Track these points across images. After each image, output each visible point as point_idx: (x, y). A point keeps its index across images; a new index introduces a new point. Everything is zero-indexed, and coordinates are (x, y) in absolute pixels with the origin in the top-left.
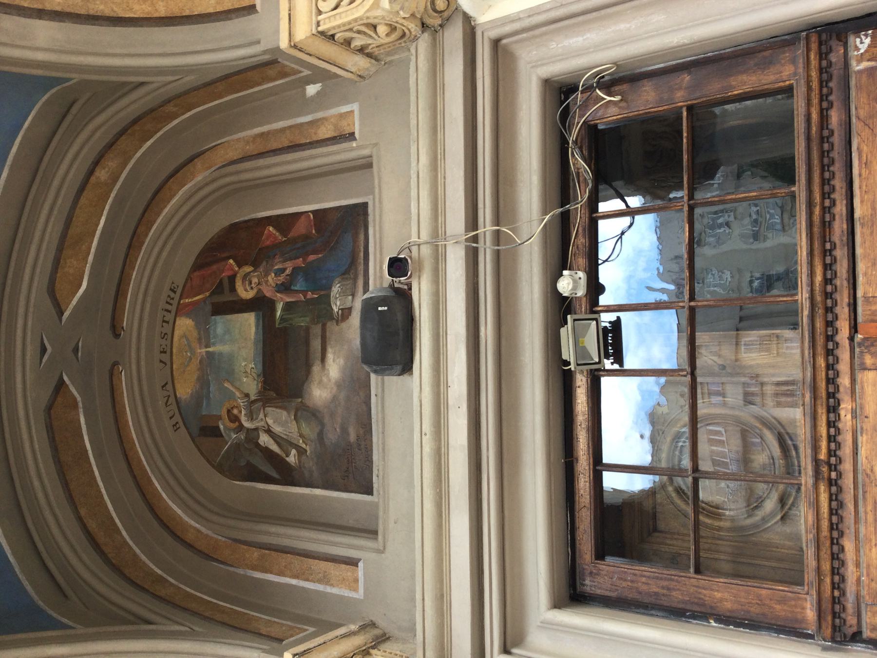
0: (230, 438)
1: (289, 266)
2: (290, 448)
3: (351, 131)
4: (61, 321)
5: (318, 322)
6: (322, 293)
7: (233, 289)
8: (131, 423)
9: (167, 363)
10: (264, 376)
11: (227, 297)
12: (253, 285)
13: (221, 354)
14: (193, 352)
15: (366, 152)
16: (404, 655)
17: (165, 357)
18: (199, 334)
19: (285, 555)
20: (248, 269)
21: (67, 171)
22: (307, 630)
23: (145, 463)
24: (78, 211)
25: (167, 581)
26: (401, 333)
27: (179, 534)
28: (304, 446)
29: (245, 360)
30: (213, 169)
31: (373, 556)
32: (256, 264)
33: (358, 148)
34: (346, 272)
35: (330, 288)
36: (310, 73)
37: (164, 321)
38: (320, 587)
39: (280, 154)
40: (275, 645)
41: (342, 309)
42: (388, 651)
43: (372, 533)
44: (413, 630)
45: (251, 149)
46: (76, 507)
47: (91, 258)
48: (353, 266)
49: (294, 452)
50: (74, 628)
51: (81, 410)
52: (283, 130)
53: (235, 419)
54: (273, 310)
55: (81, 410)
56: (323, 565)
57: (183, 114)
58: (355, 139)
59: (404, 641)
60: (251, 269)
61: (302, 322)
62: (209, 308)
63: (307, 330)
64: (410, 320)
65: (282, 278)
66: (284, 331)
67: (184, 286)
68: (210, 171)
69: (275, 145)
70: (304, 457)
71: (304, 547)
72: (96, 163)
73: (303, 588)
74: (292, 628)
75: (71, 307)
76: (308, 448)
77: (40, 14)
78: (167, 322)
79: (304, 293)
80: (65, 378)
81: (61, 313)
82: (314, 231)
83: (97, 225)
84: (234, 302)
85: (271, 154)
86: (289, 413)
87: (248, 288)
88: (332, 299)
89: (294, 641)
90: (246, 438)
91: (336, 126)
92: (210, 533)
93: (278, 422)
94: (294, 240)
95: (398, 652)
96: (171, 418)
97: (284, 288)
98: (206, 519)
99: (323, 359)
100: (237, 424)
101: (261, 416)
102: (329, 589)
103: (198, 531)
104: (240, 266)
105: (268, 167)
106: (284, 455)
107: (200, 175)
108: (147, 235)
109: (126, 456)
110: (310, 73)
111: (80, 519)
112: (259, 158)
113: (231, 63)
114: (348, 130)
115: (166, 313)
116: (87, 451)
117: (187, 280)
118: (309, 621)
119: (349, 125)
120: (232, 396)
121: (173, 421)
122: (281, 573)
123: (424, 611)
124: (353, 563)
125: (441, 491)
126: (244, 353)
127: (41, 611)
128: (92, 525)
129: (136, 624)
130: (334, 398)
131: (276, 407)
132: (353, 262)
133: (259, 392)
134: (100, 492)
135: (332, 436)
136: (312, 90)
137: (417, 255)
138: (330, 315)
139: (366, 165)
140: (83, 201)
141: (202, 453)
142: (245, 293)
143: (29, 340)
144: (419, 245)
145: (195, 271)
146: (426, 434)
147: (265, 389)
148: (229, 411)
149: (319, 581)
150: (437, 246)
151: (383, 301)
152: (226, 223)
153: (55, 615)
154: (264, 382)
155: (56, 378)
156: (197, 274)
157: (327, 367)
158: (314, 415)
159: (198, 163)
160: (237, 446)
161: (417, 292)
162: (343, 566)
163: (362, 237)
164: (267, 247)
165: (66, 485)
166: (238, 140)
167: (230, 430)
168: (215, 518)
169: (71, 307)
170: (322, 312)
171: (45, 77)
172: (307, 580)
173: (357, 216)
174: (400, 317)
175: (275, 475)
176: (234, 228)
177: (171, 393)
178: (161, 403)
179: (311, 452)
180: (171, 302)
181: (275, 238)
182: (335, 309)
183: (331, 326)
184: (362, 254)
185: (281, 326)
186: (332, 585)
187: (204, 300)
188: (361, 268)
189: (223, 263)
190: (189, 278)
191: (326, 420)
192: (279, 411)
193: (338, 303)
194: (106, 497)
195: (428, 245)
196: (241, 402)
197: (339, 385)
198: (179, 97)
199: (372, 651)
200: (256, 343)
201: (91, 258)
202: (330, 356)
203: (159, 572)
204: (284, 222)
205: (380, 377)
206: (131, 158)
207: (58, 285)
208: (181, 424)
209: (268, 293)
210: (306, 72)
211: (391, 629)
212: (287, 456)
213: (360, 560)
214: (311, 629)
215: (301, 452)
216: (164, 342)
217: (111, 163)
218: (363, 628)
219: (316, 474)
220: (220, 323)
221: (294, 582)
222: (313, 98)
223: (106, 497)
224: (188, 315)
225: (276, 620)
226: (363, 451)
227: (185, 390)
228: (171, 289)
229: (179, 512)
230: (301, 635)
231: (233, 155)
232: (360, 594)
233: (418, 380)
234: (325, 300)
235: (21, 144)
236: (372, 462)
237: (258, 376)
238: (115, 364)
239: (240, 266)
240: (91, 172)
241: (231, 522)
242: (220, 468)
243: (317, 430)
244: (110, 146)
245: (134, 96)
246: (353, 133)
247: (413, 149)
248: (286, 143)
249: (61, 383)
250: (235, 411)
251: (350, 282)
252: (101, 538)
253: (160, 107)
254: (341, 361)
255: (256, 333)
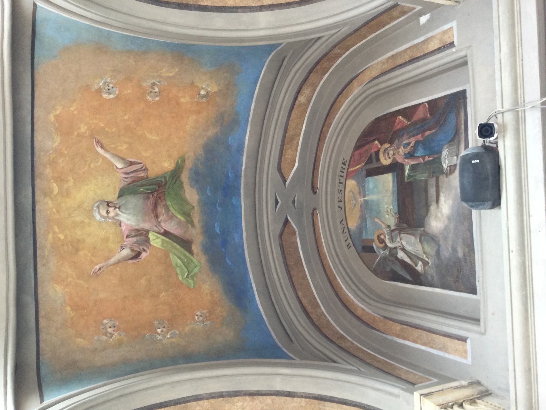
0: (380, 252)
1: (413, 141)
2: (417, 261)
3: (451, 41)
4: (285, 186)
5: (433, 176)
6: (436, 156)
7: (378, 159)
8: (324, 244)
9: (343, 208)
10: (399, 214)
11: (375, 165)
12: (390, 156)
13: (372, 201)
14: (357, 201)
15: (462, 54)
16: (502, 407)
17: (341, 204)
18: (360, 189)
19: (417, 330)
20: (387, 146)
21: (284, 99)
22: (431, 380)
23: (332, 267)
24: (290, 122)
25: (346, 338)
26: (491, 179)
27: (352, 310)
28: (427, 259)
29: (386, 204)
30: (363, 85)
31: (477, 336)
32: (391, 142)
33: (457, 51)
34: (452, 140)
35: (441, 152)
36: (421, 7)
37: (340, 183)
38: (441, 353)
39: (404, 67)
40: (410, 386)
41: (450, 166)
42: (490, 402)
43: (477, 321)
44: (508, 391)
45: (386, 67)
46: (296, 291)
47: (299, 148)
48: (457, 136)
49: (420, 263)
50: (294, 359)
51: (298, 236)
52: (405, 51)
53: (382, 241)
54: (403, 170)
55: (298, 236)
56: (442, 339)
57: (345, 53)
58: (454, 46)
59: (503, 398)
60: (389, 145)
61: (422, 177)
62: (364, 173)
63: (426, 181)
64: (497, 168)
65: (408, 149)
66: (411, 183)
67: (350, 160)
68: (361, 87)
69: (400, 61)
70: (427, 268)
71: (428, 326)
72: (298, 92)
73: (430, 353)
74: (423, 377)
75: (290, 177)
76: (429, 261)
77: (261, 8)
78: (342, 183)
79: (423, 157)
80: (289, 218)
81: (285, 181)
82: (428, 115)
83: (301, 129)
84: (379, 168)
85: (399, 68)
86: (416, 238)
87: (387, 158)
88: (442, 160)
89: (422, 386)
90: (390, 253)
91: (440, 40)
92: (370, 311)
93: (409, 244)
94: (416, 123)
95: (497, 405)
96: (346, 241)
97: (410, 155)
98: (369, 304)
99: (437, 201)
100: (384, 244)
101: (398, 239)
102: (447, 355)
103: (363, 310)
104: (381, 144)
105: (397, 76)
106: (414, 265)
107: (356, 90)
108: (328, 131)
109: (322, 263)
110: (421, 7)
111: (298, 298)
112: (391, 72)
113: (368, 13)
114: (449, 41)
115: (341, 178)
116: (301, 259)
117: (351, 156)
118: (436, 375)
119: (450, 37)
120: (380, 228)
121: (348, 242)
122: (414, 341)
123: (515, 378)
124: (463, 340)
125: (526, 294)
126: (386, 200)
127: (278, 348)
128: (305, 302)
129: (328, 362)
130: (446, 228)
131: (408, 234)
132: (457, 132)
133: (396, 224)
134: (309, 283)
135: (446, 253)
136: (423, 19)
137: (502, 121)
138: (442, 171)
139: (463, 63)
140: (293, 115)
141: (364, 263)
142: (385, 161)
143: (269, 197)
144: (503, 113)
145: (356, 150)
146: (512, 251)
147: (400, 222)
148: (378, 237)
149: (440, 349)
150: (518, 112)
151: (476, 156)
152: (373, 118)
153: (286, 351)
154: (400, 218)
155: (285, 217)
156: (357, 152)
157: (440, 206)
158: (433, 239)
159: (355, 83)
160: (384, 259)
161: (503, 148)
162: (456, 341)
163: (462, 114)
164: (398, 130)
165: (290, 278)
166: (378, 63)
167: (380, 248)
168: (372, 302)
169: (290, 177)
170: (435, 168)
171: (267, 45)
172: (432, 347)
173: (458, 100)
174: (489, 167)
175: (408, 277)
176: (378, 120)
177: (346, 227)
178: (340, 231)
179: (432, 264)
180: (343, 171)
181: (403, 123)
182: (445, 166)
183: (442, 178)
184: (463, 127)
185: (409, 181)
186: (449, 353)
187: (361, 168)
188: (463, 136)
189: (372, 144)
190: (353, 155)
191: (441, 242)
192: (409, 236)
193: (447, 162)
194: (312, 286)
195: (510, 112)
196: (385, 231)
197: (449, 219)
198: (341, 43)
199: (477, 401)
200: (393, 193)
201: (299, 148)
202: (442, 199)
203: (342, 332)
204: (408, 112)
205: (478, 211)
206: (317, 86)
207: (282, 166)
208: (351, 244)
209: (400, 160)
210: (419, 8)
211: (492, 388)
212: (416, 266)
213: (468, 338)
214: (435, 380)
215: (425, 264)
216: (340, 195)
217: (306, 91)
218: (471, 384)
219: (436, 278)
220: (371, 181)
221: (424, 348)
222: (425, 25)
223: (312, 286)
224: (353, 178)
225: (413, 371)
226: (469, 264)
227: (353, 224)
228: (343, 163)
229: (352, 297)
230: (428, 383)
231: (375, 73)
232: (468, 361)
233: (505, 212)
234: (438, 161)
235: (260, 86)
236: (475, 272)
237: (395, 214)
238: (315, 209)
239: (381, 144)
240: (296, 99)
241: (385, 307)
242: (375, 272)
243: (435, 249)
244: (305, 81)
245: (315, 47)
246: (453, 42)
247: (496, 44)
248: (408, 59)
249: (286, 222)
250: (382, 237)
251: (455, 146)
252: (309, 308)
253: (330, 51)
254: (451, 202)
255: (393, 186)
